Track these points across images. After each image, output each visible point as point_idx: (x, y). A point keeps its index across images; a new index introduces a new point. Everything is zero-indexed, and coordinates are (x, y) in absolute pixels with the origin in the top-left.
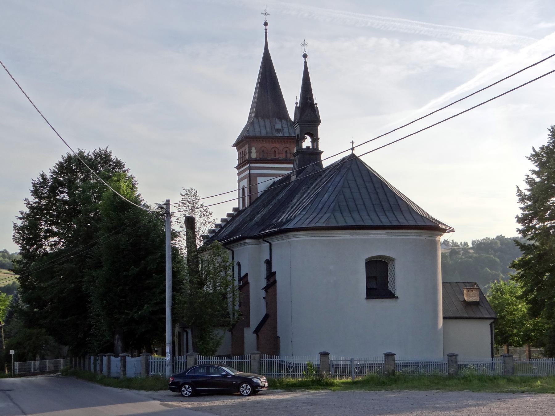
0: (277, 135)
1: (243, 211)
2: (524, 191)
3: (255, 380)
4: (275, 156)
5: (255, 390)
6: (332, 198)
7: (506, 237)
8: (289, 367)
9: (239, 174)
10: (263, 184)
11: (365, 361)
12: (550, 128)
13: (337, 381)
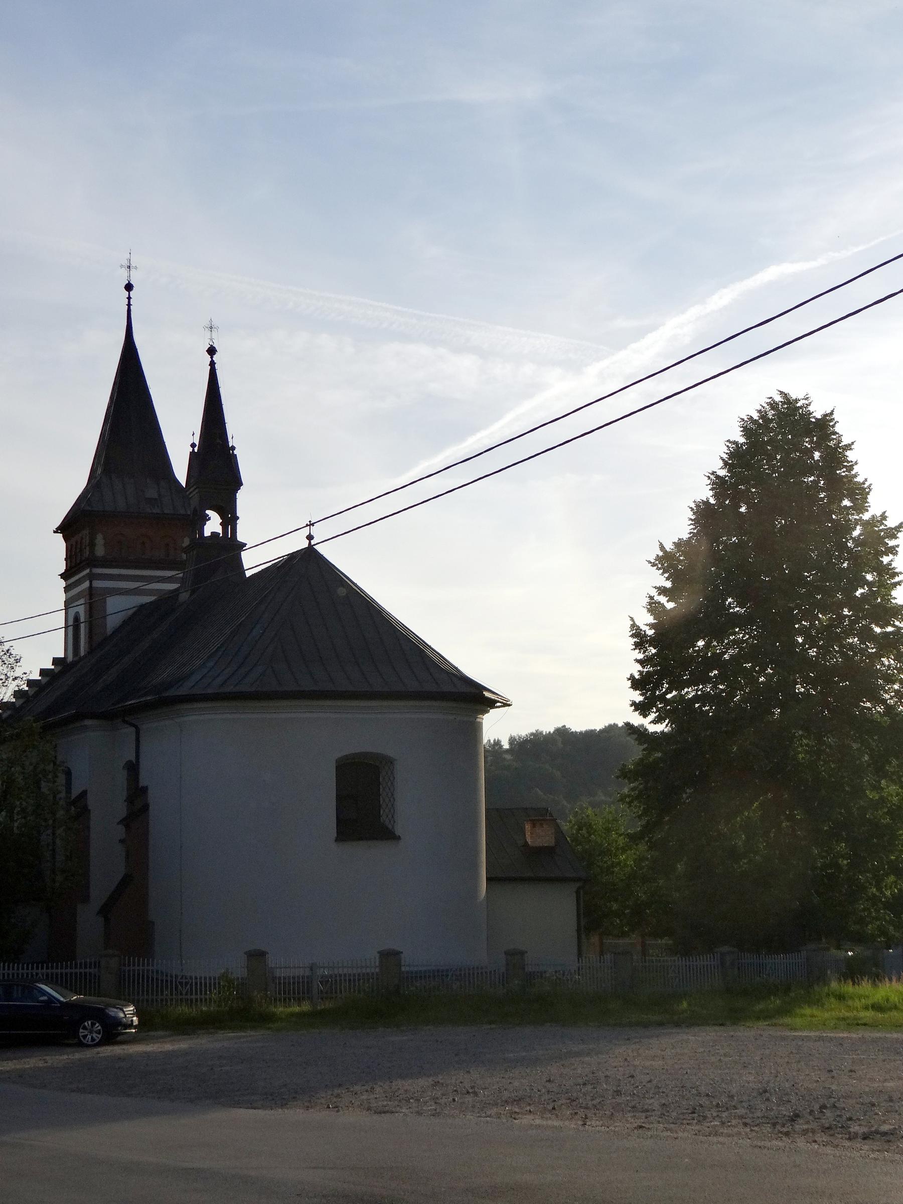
1: (73, 664)
2: (644, 628)
3: (112, 1012)
5: (112, 1032)
7: (573, 730)
9: (67, 589)
10: (118, 608)
11: (362, 967)
12: (693, 505)
13: (280, 1010)
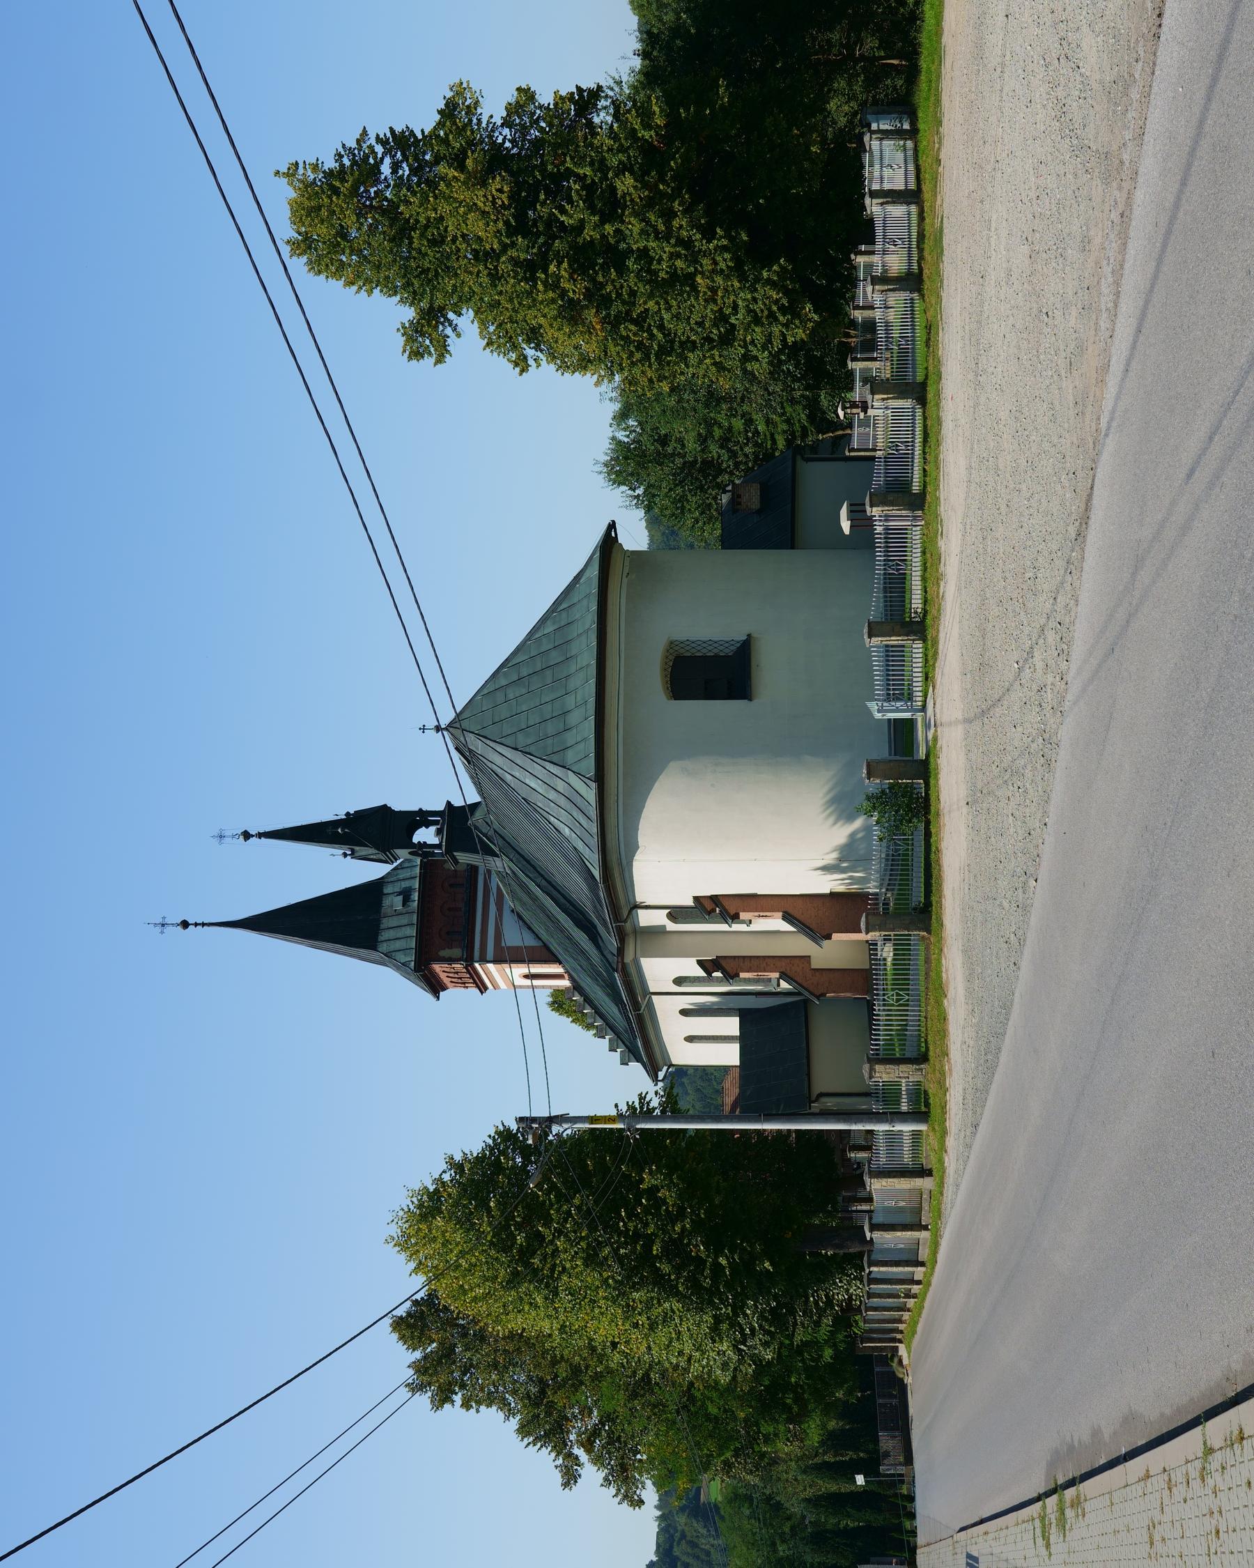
6: (537, 770)
8: (896, 850)
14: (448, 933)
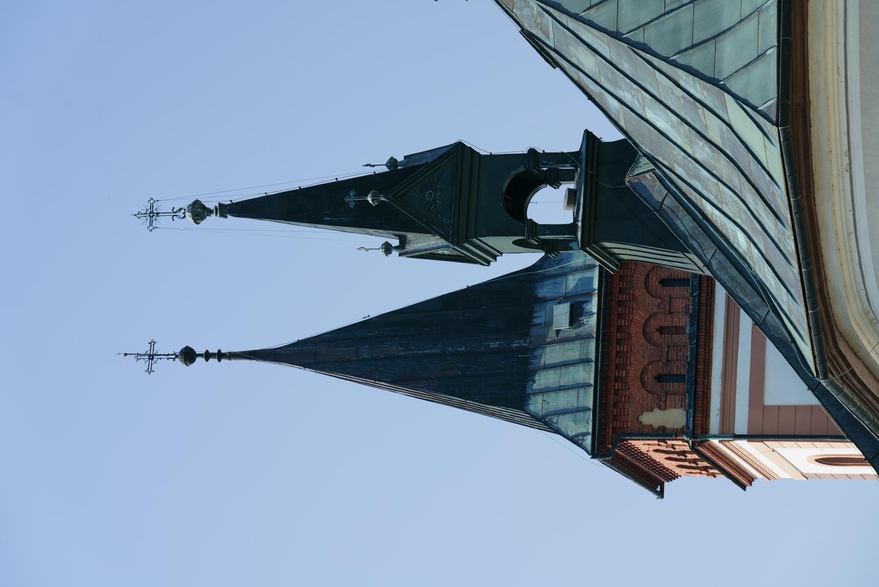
0: (593, 321)
4: (679, 330)
6: (662, 86)
14: (659, 378)
